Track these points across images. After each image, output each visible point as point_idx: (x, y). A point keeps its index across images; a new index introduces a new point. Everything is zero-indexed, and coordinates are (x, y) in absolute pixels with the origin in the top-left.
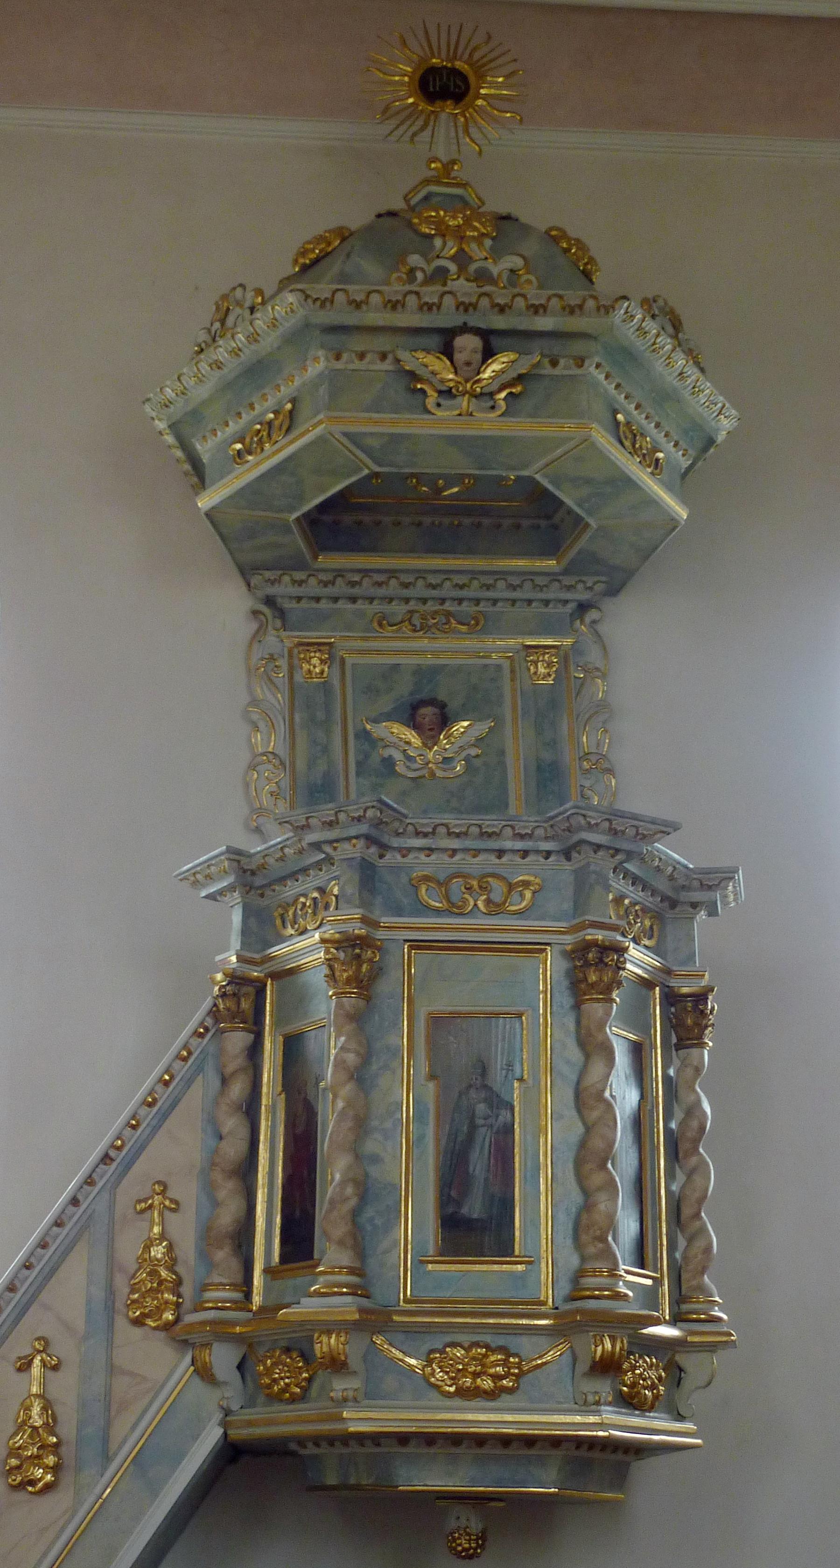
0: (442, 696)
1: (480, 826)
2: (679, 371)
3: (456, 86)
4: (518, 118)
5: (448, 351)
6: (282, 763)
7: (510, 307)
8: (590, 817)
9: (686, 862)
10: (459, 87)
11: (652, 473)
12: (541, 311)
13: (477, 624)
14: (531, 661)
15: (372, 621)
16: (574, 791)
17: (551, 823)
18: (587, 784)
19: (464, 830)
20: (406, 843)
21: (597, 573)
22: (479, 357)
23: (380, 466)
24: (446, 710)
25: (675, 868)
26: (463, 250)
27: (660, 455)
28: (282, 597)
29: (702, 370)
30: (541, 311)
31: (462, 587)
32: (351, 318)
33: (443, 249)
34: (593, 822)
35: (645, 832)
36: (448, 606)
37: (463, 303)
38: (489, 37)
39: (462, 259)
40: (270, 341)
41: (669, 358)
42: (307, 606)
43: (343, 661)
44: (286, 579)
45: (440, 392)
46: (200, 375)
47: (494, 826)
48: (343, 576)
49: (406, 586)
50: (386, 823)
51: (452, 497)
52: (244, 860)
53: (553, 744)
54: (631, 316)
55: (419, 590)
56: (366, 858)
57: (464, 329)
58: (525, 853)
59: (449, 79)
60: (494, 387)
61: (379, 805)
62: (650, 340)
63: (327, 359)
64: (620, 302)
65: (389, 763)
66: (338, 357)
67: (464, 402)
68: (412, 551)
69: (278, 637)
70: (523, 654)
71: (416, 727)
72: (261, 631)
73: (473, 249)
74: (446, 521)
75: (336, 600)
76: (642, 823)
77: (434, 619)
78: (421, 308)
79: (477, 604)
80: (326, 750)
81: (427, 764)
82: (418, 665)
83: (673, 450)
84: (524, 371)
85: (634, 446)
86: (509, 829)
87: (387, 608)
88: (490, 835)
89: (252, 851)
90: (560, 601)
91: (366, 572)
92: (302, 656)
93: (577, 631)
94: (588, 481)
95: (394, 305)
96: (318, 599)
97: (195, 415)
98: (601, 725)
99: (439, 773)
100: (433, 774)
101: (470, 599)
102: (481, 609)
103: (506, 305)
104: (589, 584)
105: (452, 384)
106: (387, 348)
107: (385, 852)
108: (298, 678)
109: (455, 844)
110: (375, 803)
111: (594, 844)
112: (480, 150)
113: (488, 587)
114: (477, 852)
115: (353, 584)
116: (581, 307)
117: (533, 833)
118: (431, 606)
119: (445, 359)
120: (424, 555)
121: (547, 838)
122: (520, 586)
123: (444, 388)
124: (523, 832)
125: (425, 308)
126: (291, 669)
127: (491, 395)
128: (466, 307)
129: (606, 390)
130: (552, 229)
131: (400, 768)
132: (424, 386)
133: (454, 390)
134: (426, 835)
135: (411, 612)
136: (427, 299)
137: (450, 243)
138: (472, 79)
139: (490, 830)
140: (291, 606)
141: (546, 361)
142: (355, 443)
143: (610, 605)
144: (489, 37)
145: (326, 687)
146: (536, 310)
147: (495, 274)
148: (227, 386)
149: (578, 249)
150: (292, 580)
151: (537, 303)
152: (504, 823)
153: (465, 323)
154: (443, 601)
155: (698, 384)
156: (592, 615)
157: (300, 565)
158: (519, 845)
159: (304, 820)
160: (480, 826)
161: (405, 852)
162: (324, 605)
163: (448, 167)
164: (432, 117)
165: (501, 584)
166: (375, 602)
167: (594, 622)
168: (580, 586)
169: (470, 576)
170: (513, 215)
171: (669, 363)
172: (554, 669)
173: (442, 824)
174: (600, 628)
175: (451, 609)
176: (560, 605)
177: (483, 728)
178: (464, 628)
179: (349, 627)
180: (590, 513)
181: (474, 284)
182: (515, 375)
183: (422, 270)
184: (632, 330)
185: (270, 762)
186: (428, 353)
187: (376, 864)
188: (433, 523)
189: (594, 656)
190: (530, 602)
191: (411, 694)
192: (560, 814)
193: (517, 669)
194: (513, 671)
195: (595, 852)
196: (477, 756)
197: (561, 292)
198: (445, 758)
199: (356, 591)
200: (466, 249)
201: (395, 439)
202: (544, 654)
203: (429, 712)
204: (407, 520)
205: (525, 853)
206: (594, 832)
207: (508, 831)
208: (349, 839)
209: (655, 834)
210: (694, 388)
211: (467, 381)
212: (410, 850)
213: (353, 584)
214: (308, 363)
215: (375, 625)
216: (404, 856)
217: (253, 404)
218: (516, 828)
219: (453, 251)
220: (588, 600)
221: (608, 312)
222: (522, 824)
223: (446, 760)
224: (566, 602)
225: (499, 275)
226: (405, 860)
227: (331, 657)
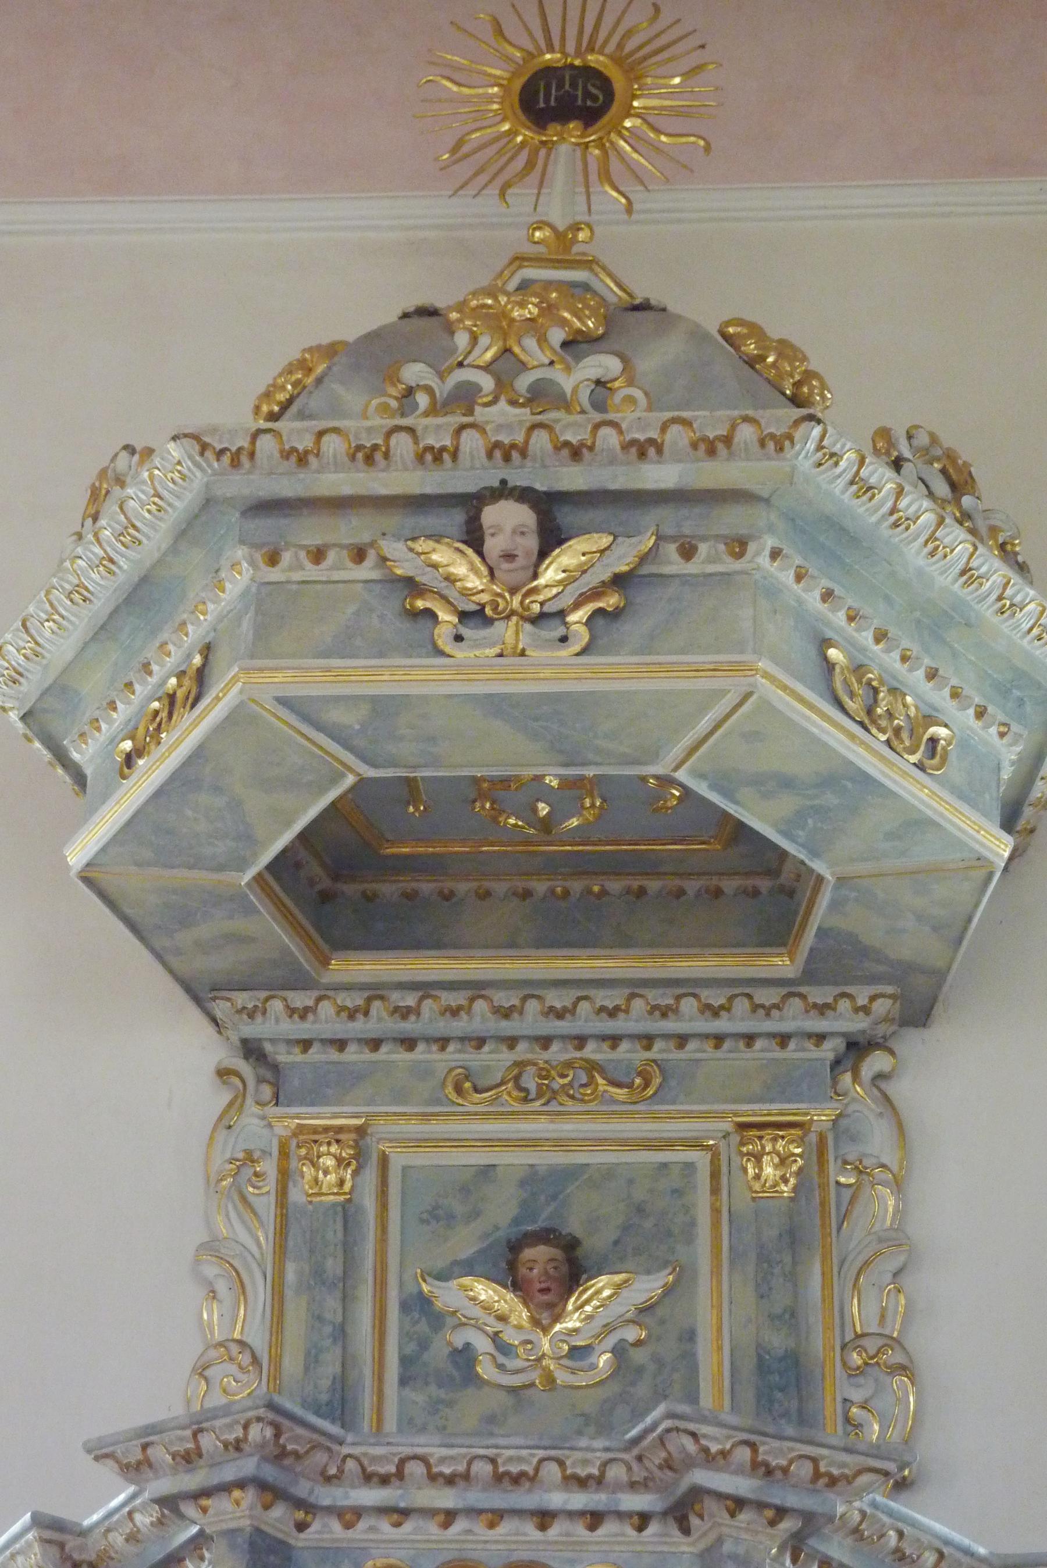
0: (574, 1225)
1: (493, 1461)
2: (961, 565)
3: (587, 94)
4: (702, 143)
5: (474, 538)
6: (255, 1360)
7: (591, 448)
8: (705, 1436)
9: (967, 1542)
10: (595, 98)
11: (920, 766)
12: (652, 451)
13: (647, 1084)
14: (748, 1154)
15: (443, 1084)
16: (831, 1411)
17: (636, 1451)
18: (857, 1396)
19: (461, 1468)
20: (311, 1491)
21: (873, 979)
22: (531, 543)
23: (374, 765)
24: (579, 1252)
25: (941, 1555)
26: (507, 350)
27: (942, 732)
28: (272, 1041)
29: (1022, 568)
30: (652, 451)
31: (613, 1013)
32: (289, 485)
33: (470, 353)
34: (714, 1448)
35: (835, 1472)
36: (591, 1051)
37: (497, 445)
38: (657, 9)
39: (506, 366)
40: (156, 539)
41: (932, 538)
42: (323, 1057)
43: (384, 1161)
44: (277, 1005)
45: (464, 616)
46: (56, 617)
47: (520, 1459)
48: (382, 998)
49: (506, 1013)
50: (297, 1456)
51: (580, 836)
52: (72, 1542)
53: (790, 1318)
54: (832, 455)
55: (531, 1021)
56: (264, 1527)
57: (502, 491)
58: (595, 1519)
59: (574, 85)
60: (567, 601)
61: (271, 1416)
62: (882, 504)
63: (252, 563)
64: (804, 426)
65: (465, 1356)
66: (273, 560)
67: (506, 631)
68: (512, 945)
69: (263, 1118)
70: (735, 1139)
71: (517, 1286)
72: (236, 1105)
73: (530, 350)
74: (576, 886)
75: (375, 1044)
76: (825, 1452)
77: (563, 1076)
78: (420, 458)
79: (648, 1048)
80: (342, 1333)
81: (539, 1360)
82: (532, 1166)
83: (977, 725)
84: (625, 568)
85: (870, 712)
86: (553, 1468)
87: (475, 1059)
88: (517, 1479)
89: (87, 1523)
90: (809, 1036)
91: (426, 989)
92: (303, 1152)
93: (845, 1095)
94: (787, 783)
95: (369, 456)
96: (341, 1044)
97: (60, 689)
98: (889, 1277)
99: (562, 1377)
100: (550, 1380)
101: (631, 1037)
102: (658, 1056)
103: (582, 444)
104: (862, 1001)
105: (485, 598)
106: (365, 538)
107: (309, 1518)
108: (296, 1195)
109: (447, 1499)
110: (261, 1412)
111: (727, 1497)
112: (629, 202)
113: (665, 1012)
114: (496, 1517)
115: (404, 1013)
116: (727, 440)
117: (603, 1473)
118: (557, 1053)
119: (469, 551)
120: (532, 952)
121: (633, 1486)
122: (727, 1008)
123: (473, 607)
124: (582, 1472)
125: (429, 457)
126: (285, 1176)
127: (561, 614)
128: (505, 452)
129: (800, 602)
130: (728, 323)
131: (485, 1370)
132: (428, 605)
133: (488, 611)
134: (385, 1480)
135: (520, 1065)
136: (431, 441)
137: (484, 340)
138: (619, 83)
139: (514, 1469)
140: (290, 1058)
141: (671, 550)
142: (306, 718)
143: (912, 1044)
144: (657, 9)
145: (347, 1212)
146: (643, 450)
147: (568, 391)
148: (104, 631)
149: (780, 355)
150: (287, 1007)
151: (641, 437)
152: (541, 1453)
153: (503, 482)
154: (580, 1041)
155: (1009, 592)
156: (877, 1062)
157: (300, 982)
158: (579, 1500)
159: (139, 1450)
160: (493, 1461)
161: (350, 1516)
162: (353, 1054)
163: (564, 238)
164: (543, 152)
165: (688, 1005)
166: (451, 1048)
167: (880, 1077)
168: (844, 1005)
169: (627, 991)
170: (653, 302)
171: (937, 548)
172: (794, 1168)
173: (415, 1457)
174: (891, 1088)
175: (597, 1057)
176: (809, 1045)
177: (648, 1287)
178: (620, 1093)
179: (400, 1096)
180: (815, 854)
181: (528, 410)
182: (606, 576)
183: (429, 390)
184: (841, 483)
185: (231, 1359)
186: (438, 542)
187: (292, 1542)
188: (552, 891)
189: (878, 1142)
190: (750, 1039)
191: (516, 1221)
192: (647, 1432)
193: (724, 1169)
194: (715, 1175)
195: (733, 1515)
196: (639, 1343)
197: (685, 414)
198: (573, 1349)
199: (410, 1026)
200: (517, 350)
201: (383, 708)
202: (774, 1140)
203: (547, 1259)
204: (500, 888)
205: (595, 1519)
206: (719, 1470)
207: (552, 1471)
208: (225, 1488)
209: (859, 1473)
210: (1000, 598)
211: (513, 591)
212: (358, 1512)
213: (404, 1013)
214: (223, 574)
215: (450, 1090)
216: (348, 1526)
217: (149, 664)
218: (568, 1463)
219: (489, 355)
220: (864, 1032)
221: (781, 449)
222: (578, 1455)
223: (576, 1352)
224: (820, 1038)
225: (575, 390)
226: (350, 1534)
227: (360, 1156)
